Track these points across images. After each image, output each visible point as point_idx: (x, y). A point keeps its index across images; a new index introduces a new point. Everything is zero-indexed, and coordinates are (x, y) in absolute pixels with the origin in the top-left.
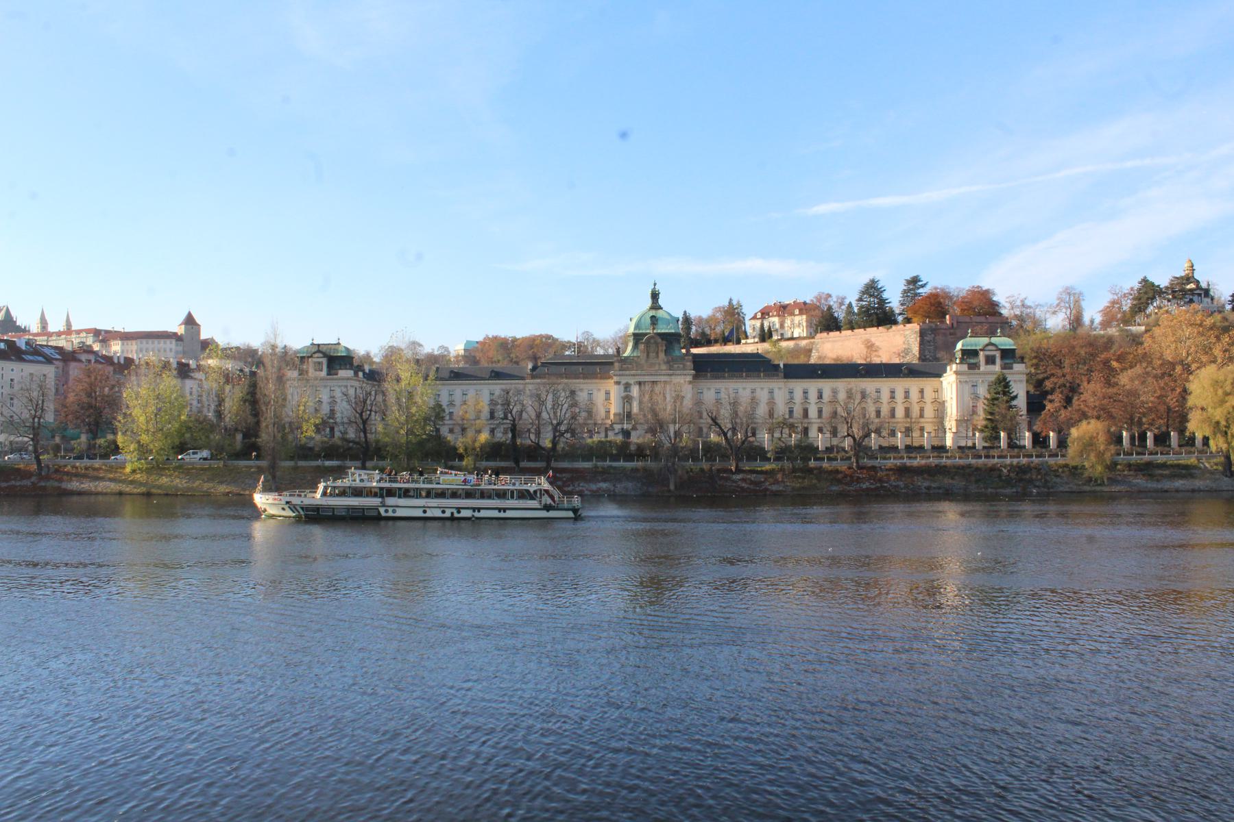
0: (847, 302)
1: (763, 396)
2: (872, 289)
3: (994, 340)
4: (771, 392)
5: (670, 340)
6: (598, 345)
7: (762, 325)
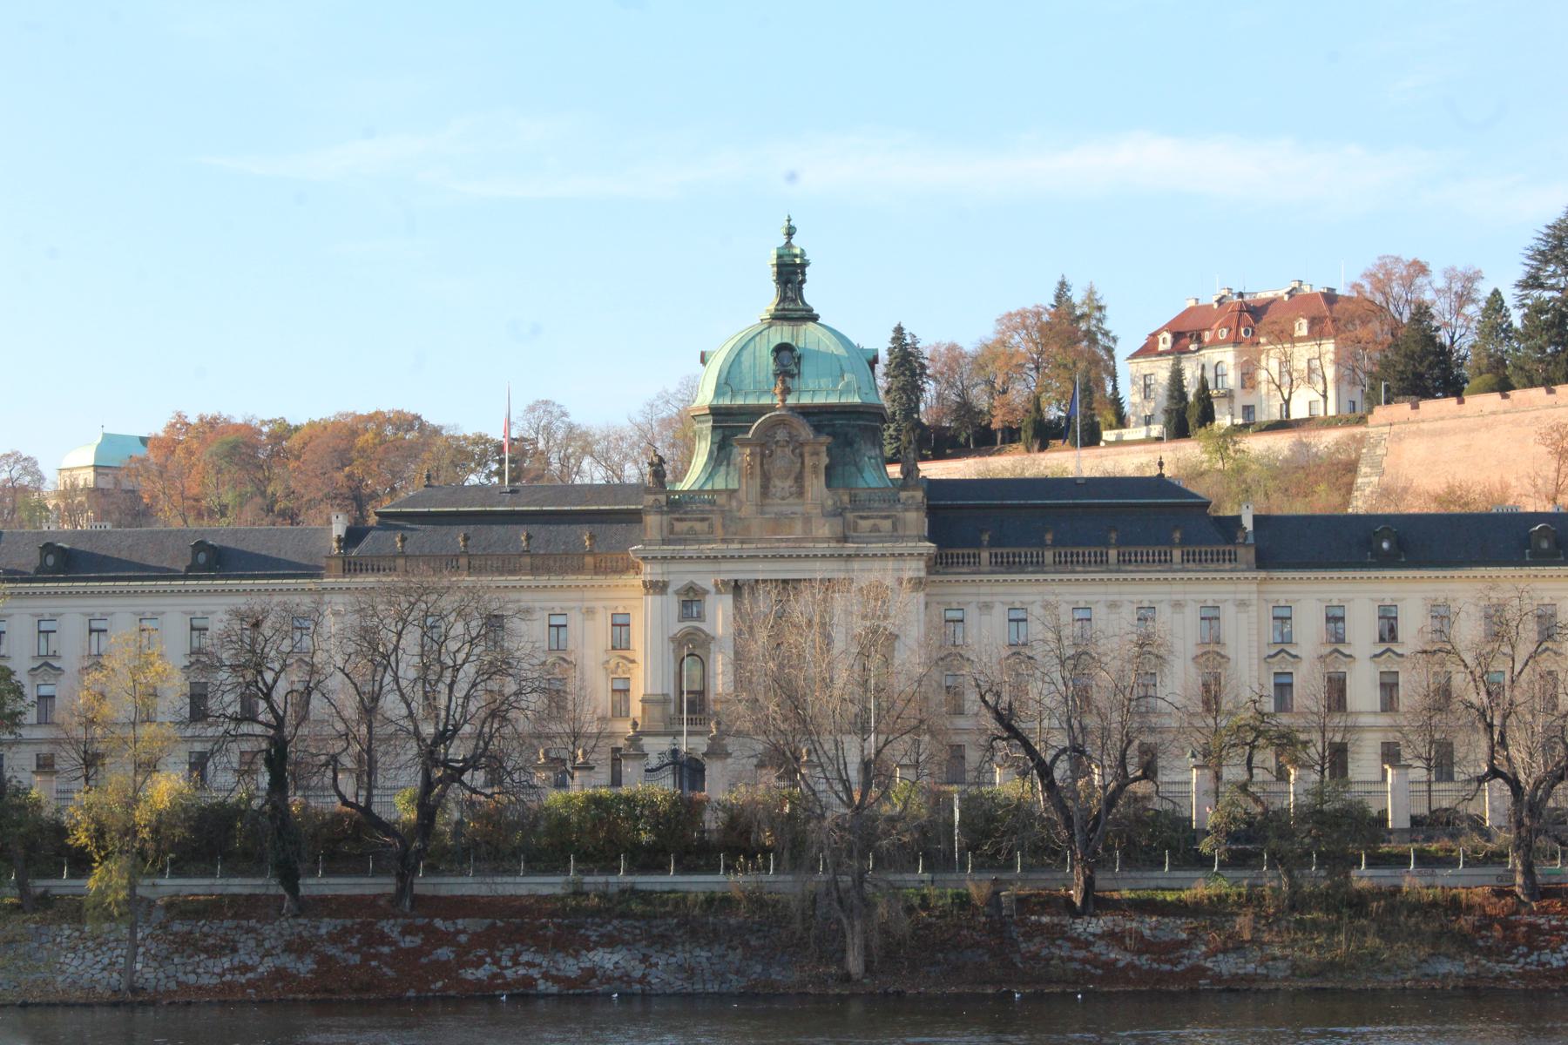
4: (1211, 617)
5: (845, 429)
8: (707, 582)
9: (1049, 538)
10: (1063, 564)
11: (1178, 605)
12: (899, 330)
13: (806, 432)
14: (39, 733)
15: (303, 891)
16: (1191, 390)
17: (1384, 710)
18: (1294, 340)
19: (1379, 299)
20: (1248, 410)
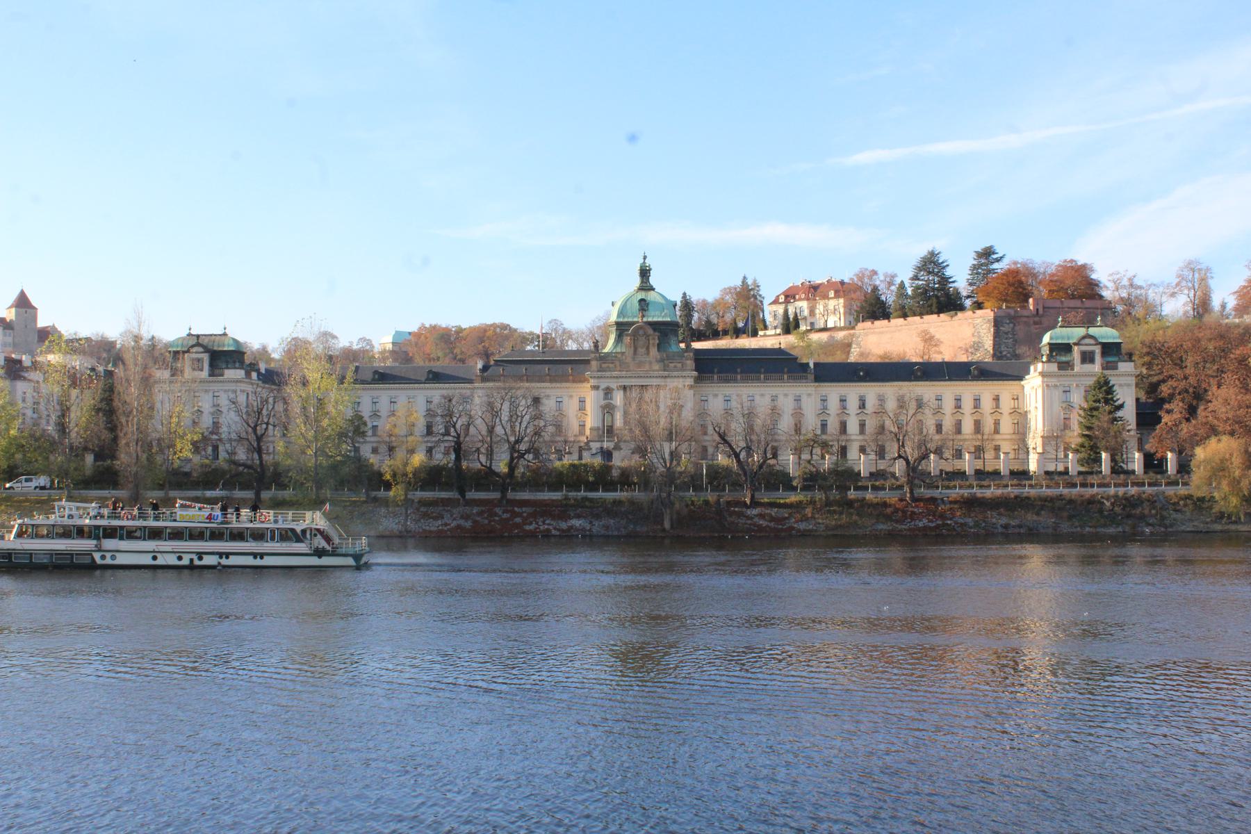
1: (786, 404)
2: (931, 264)
3: (1092, 331)
4: (798, 400)
5: (664, 331)
6: (570, 337)
7: (786, 311)
8: (614, 386)
10: (744, 380)
11: (786, 395)
13: (650, 331)
14: (373, 439)
16: (791, 317)
18: (829, 298)
20: (812, 324)
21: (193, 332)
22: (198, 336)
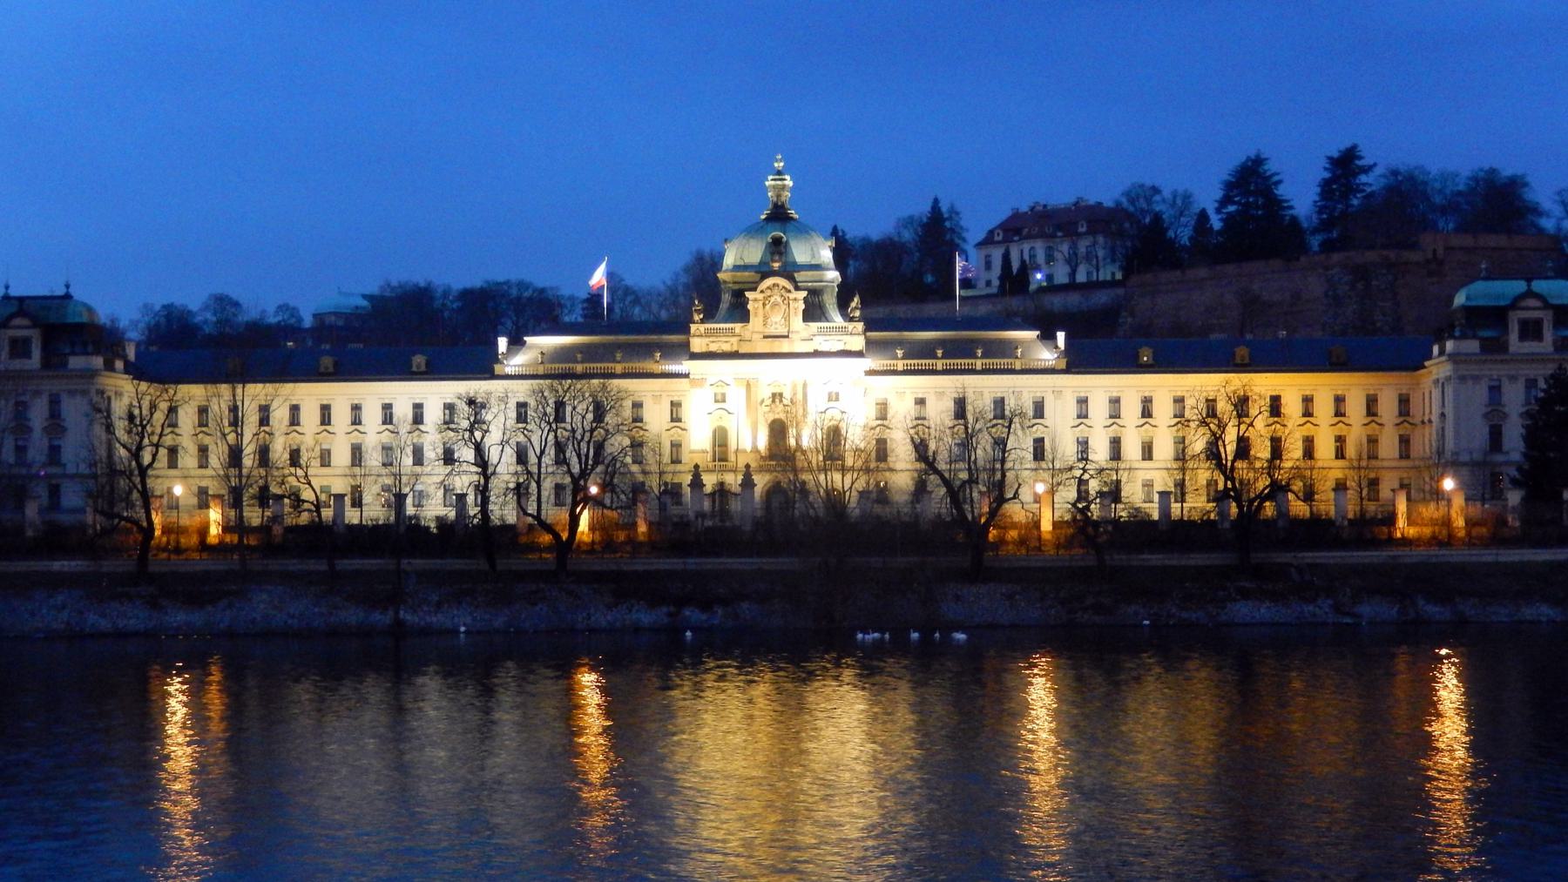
0: (1196, 209)
2: (1251, 181)
6: (637, 301)
7: (1006, 258)
9: (979, 352)
12: (936, 201)
15: (499, 568)
16: (1015, 265)
17: (1401, 457)
18: (1080, 235)
19: (1131, 209)
21: (13, 292)
22: (21, 299)
